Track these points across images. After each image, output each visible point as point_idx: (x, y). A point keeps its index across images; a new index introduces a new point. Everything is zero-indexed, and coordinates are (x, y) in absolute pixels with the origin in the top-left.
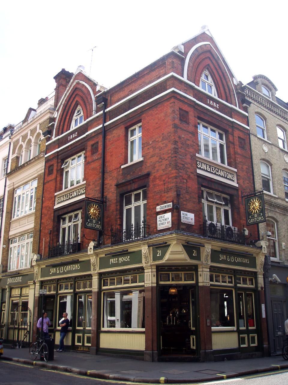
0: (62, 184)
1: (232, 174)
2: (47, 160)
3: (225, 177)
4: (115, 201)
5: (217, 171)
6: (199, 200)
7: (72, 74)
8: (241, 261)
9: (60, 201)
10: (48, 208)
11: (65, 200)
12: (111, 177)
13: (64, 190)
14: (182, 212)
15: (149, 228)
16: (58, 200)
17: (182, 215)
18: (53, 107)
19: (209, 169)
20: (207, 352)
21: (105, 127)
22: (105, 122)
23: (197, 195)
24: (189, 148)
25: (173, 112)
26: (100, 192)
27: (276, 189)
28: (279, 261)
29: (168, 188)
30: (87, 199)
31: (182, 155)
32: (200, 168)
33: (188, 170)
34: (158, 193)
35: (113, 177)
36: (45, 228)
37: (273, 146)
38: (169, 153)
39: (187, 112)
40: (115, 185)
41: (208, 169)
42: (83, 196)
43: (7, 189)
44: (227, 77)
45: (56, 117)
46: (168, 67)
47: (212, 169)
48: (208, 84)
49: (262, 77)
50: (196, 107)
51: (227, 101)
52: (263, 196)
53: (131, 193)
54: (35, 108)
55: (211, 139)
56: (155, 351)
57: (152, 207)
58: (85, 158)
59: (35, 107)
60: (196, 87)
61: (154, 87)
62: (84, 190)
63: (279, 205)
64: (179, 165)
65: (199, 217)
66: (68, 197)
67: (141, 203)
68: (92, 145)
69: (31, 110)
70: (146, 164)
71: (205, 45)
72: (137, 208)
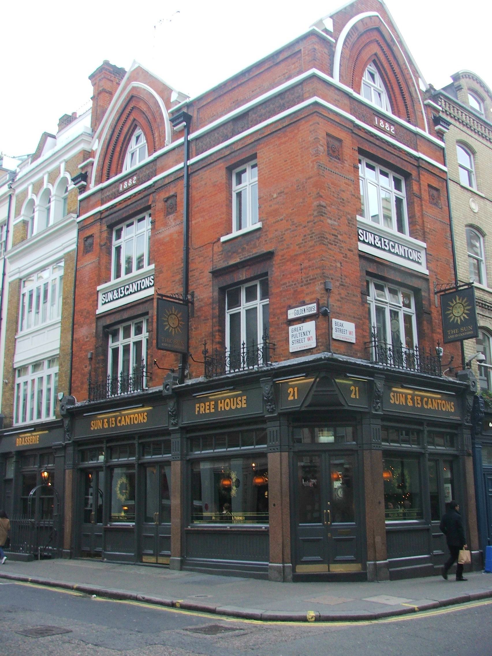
0: (109, 270)
2: (82, 227)
3: (407, 256)
4: (211, 300)
5: (393, 247)
9: (107, 301)
10: (85, 314)
11: (117, 299)
12: (202, 258)
13: (113, 281)
14: (334, 320)
15: (274, 349)
16: (104, 299)
17: (334, 326)
18: (90, 131)
19: (379, 242)
20: (379, 564)
21: (188, 167)
22: (188, 159)
23: (359, 290)
24: (344, 206)
26: (182, 284)
30: (159, 297)
32: (364, 242)
35: (206, 258)
36: (81, 348)
38: (310, 215)
39: (340, 141)
42: (151, 292)
43: (8, 280)
44: (407, 77)
45: (97, 150)
47: (385, 242)
48: (374, 90)
49: (469, 76)
50: (356, 131)
51: (409, 122)
53: (238, 286)
54: (54, 133)
59: (53, 130)
60: (355, 95)
61: (281, 95)
64: (327, 236)
65: (363, 330)
66: (121, 293)
67: (258, 303)
68: (165, 200)
69: (46, 135)
70: (266, 235)
71: (370, 17)
72: (251, 313)
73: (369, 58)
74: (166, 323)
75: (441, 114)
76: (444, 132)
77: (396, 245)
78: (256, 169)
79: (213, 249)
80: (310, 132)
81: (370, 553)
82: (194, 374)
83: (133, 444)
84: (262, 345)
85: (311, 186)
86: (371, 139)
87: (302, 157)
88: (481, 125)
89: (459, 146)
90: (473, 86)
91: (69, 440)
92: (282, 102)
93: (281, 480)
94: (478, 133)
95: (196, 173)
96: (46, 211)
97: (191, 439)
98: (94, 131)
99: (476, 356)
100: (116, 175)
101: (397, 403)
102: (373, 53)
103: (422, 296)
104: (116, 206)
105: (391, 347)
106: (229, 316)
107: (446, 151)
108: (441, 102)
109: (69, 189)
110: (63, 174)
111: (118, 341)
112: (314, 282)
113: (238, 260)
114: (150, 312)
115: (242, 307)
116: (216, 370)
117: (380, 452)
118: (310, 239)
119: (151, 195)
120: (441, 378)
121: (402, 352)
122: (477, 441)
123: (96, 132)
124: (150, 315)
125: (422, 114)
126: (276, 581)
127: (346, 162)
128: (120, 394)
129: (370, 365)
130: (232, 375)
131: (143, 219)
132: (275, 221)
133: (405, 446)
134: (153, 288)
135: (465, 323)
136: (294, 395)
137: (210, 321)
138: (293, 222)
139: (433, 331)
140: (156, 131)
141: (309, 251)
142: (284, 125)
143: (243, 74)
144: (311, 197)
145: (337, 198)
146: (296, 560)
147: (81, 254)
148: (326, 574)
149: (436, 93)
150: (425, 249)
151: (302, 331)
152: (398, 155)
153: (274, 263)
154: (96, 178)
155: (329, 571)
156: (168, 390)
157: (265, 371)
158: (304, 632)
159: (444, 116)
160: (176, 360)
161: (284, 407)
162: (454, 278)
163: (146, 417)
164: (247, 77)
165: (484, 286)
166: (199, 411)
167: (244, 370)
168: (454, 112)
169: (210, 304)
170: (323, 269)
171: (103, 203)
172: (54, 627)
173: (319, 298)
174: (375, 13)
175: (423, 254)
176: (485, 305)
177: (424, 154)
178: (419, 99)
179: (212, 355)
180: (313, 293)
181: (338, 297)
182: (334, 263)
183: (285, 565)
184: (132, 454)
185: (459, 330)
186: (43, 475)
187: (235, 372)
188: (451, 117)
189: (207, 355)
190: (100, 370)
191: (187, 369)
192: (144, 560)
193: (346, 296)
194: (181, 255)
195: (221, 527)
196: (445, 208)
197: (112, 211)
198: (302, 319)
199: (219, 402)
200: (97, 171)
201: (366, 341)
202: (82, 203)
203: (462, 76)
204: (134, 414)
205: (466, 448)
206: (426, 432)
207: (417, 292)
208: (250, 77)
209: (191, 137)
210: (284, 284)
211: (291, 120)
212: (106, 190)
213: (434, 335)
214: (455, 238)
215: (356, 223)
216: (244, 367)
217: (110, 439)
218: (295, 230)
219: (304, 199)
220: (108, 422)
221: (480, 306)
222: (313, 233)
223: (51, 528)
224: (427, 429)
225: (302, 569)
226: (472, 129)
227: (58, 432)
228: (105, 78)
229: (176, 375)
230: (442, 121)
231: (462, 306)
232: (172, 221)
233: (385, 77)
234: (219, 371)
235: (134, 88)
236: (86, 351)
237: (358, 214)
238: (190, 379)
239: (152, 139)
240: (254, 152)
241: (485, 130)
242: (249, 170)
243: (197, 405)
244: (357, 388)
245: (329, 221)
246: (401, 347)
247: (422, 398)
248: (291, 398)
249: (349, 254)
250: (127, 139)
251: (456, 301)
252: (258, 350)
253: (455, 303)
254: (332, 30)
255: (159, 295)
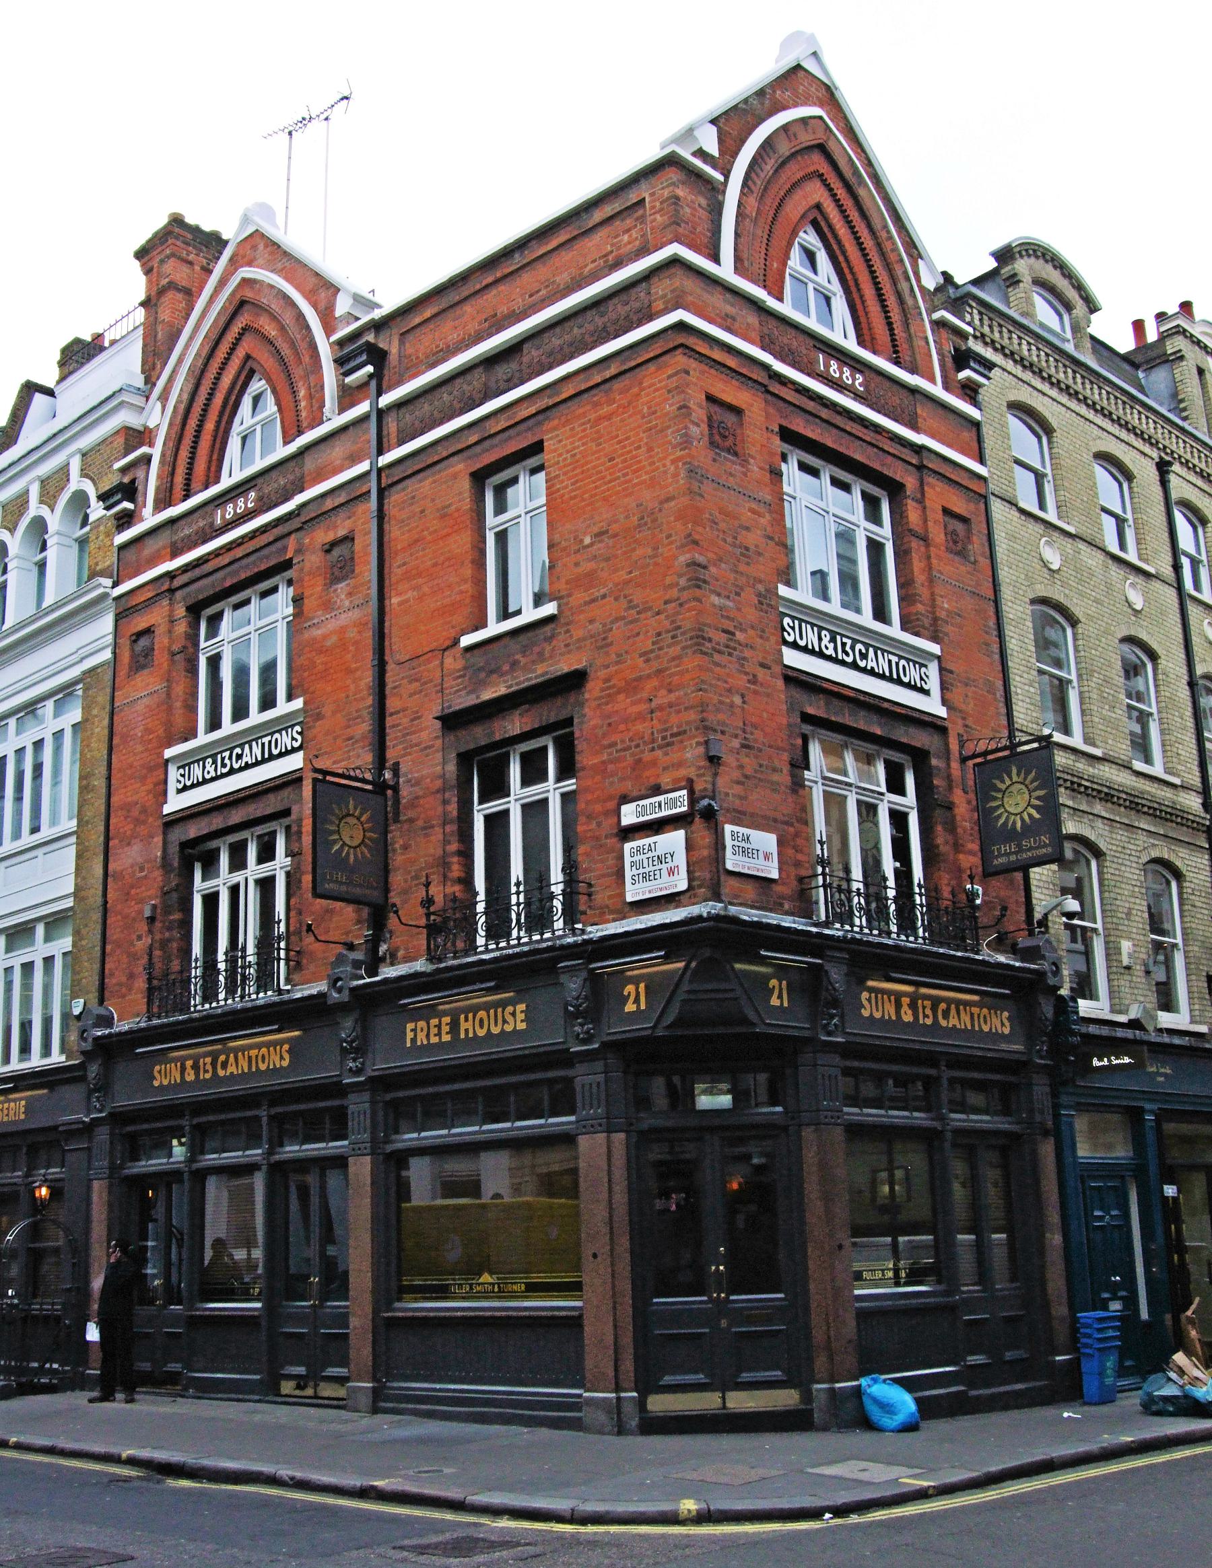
0: (193, 709)
1: (922, 665)
2: (125, 610)
3: (895, 676)
4: (439, 783)
5: (864, 656)
6: (793, 775)
7: (214, 242)
8: (973, 1025)
9: (189, 783)
11: (213, 779)
12: (418, 684)
13: (203, 738)
14: (728, 828)
15: (590, 895)
16: (181, 779)
17: (729, 842)
18: (139, 381)
19: (831, 646)
21: (380, 471)
22: (380, 452)
23: (786, 756)
24: (748, 564)
25: (684, 410)
27: (1096, 720)
28: (1107, 1015)
29: (666, 730)
31: (724, 593)
32: (794, 645)
33: (747, 653)
34: (625, 750)
36: (128, 894)
37: (1082, 546)
38: (671, 586)
39: (737, 411)
40: (437, 718)
41: (827, 648)
42: (295, 762)
44: (892, 257)
46: (655, 220)
47: (844, 645)
49: (1034, 251)
50: (775, 388)
51: (897, 362)
52: (1051, 759)
54: (49, 381)
55: (833, 518)
56: (626, 1391)
57: (598, 808)
58: (297, 601)
59: (48, 376)
60: (772, 303)
62: (299, 738)
63: (1109, 788)
64: (710, 633)
66: (224, 765)
67: (552, 790)
68: (327, 547)
69: (30, 389)
72: (535, 811)
73: (803, 216)
74: (336, 837)
75: (971, 343)
76: (980, 386)
77: (871, 650)
78: (541, 476)
79: (442, 663)
80: (669, 391)
81: (821, 1362)
82: (401, 953)
83: (257, 1119)
84: (561, 886)
85: (672, 519)
86: (810, 405)
87: (650, 449)
88: (1065, 366)
89: (1015, 416)
90: (1045, 276)
91: (101, 1111)
92: (599, 321)
93: (610, 1197)
94: (1057, 385)
95: (400, 486)
96: (35, 570)
97: (394, 1105)
98: (150, 381)
99: (1059, 904)
100: (206, 488)
101: (878, 1015)
102: (812, 203)
103: (930, 767)
104: (207, 561)
105: (861, 886)
106: (482, 819)
107: (985, 430)
108: (971, 314)
109: (92, 518)
110: (76, 482)
111: (218, 876)
112: (682, 742)
113: (502, 690)
114: (295, 809)
115: (512, 798)
116: (454, 944)
117: (839, 1130)
118: (670, 641)
119: (293, 536)
120: (977, 957)
121: (887, 899)
122: (1064, 1099)
123: (154, 385)
124: (294, 816)
125: (927, 343)
126: (601, 1432)
127: (752, 461)
128: (223, 1001)
129: (814, 930)
130: (492, 955)
131: (274, 590)
132: (587, 599)
133: (898, 1116)
134: (301, 754)
135: (1030, 829)
136: (637, 1001)
137: (438, 830)
138: (631, 601)
139: (957, 847)
140: (300, 384)
141: (667, 669)
142: (608, 374)
143: (506, 253)
144: (672, 543)
145: (734, 545)
146: (647, 1385)
147: (123, 672)
148: (715, 1415)
149: (960, 293)
150: (939, 658)
151: (654, 854)
152: (874, 441)
153: (587, 696)
154: (157, 493)
155: (724, 1407)
156: (339, 991)
157: (569, 946)
158: (676, 1546)
159: (978, 347)
160: (359, 922)
161: (616, 1030)
162: (1005, 723)
163: (287, 1056)
164: (518, 260)
165: (1076, 741)
166: (414, 1040)
167: (519, 945)
168: (1002, 337)
169: (438, 791)
170: (702, 712)
171: (175, 553)
172: (90, 1549)
173: (695, 778)
174: (816, 111)
175: (933, 670)
176: (1080, 785)
177: (933, 436)
178: (919, 308)
179: (445, 911)
180: (680, 764)
181: (736, 774)
182: (728, 697)
183: (623, 1395)
184: (253, 1140)
185: (1019, 846)
186: (37, 1195)
187: (498, 949)
188: (995, 349)
189: (432, 909)
190: (175, 945)
191: (385, 942)
192: (284, 1391)
193: (756, 771)
194: (367, 678)
195: (470, 1309)
196: (984, 562)
197: (197, 572)
198: (655, 827)
199: (462, 1016)
200: (159, 477)
201: (804, 873)
202: (124, 553)
203: (1020, 252)
204: (259, 1046)
205: (1038, 1118)
206: (945, 1082)
207: (920, 758)
208: (525, 262)
209: (385, 400)
210: (611, 746)
211: (623, 363)
212: (182, 522)
213: (961, 856)
214: (1009, 631)
215: (777, 603)
216: (519, 938)
217: (199, 1107)
218: (636, 620)
219: (656, 549)
220: (196, 1067)
221: (1066, 788)
222: (679, 627)
223: (58, 1319)
224: (947, 1074)
225: (659, 1404)
226: (1045, 375)
227: (72, 1094)
228: (173, 255)
229: (359, 955)
230: (975, 360)
231: (1025, 790)
232: (343, 596)
233: (841, 259)
234: (460, 945)
235: (245, 282)
236: (142, 901)
237: (781, 582)
238: (392, 964)
239: (292, 405)
240: (536, 439)
241: (1074, 378)
242: (523, 479)
243: (410, 1026)
244: (784, 982)
245: (715, 600)
246: (886, 887)
247: (936, 1002)
248: (630, 1007)
249: (761, 674)
250: (231, 402)
251: (1011, 779)
252: (552, 896)
253: (1008, 782)
254: (716, 154)
255: (316, 770)
